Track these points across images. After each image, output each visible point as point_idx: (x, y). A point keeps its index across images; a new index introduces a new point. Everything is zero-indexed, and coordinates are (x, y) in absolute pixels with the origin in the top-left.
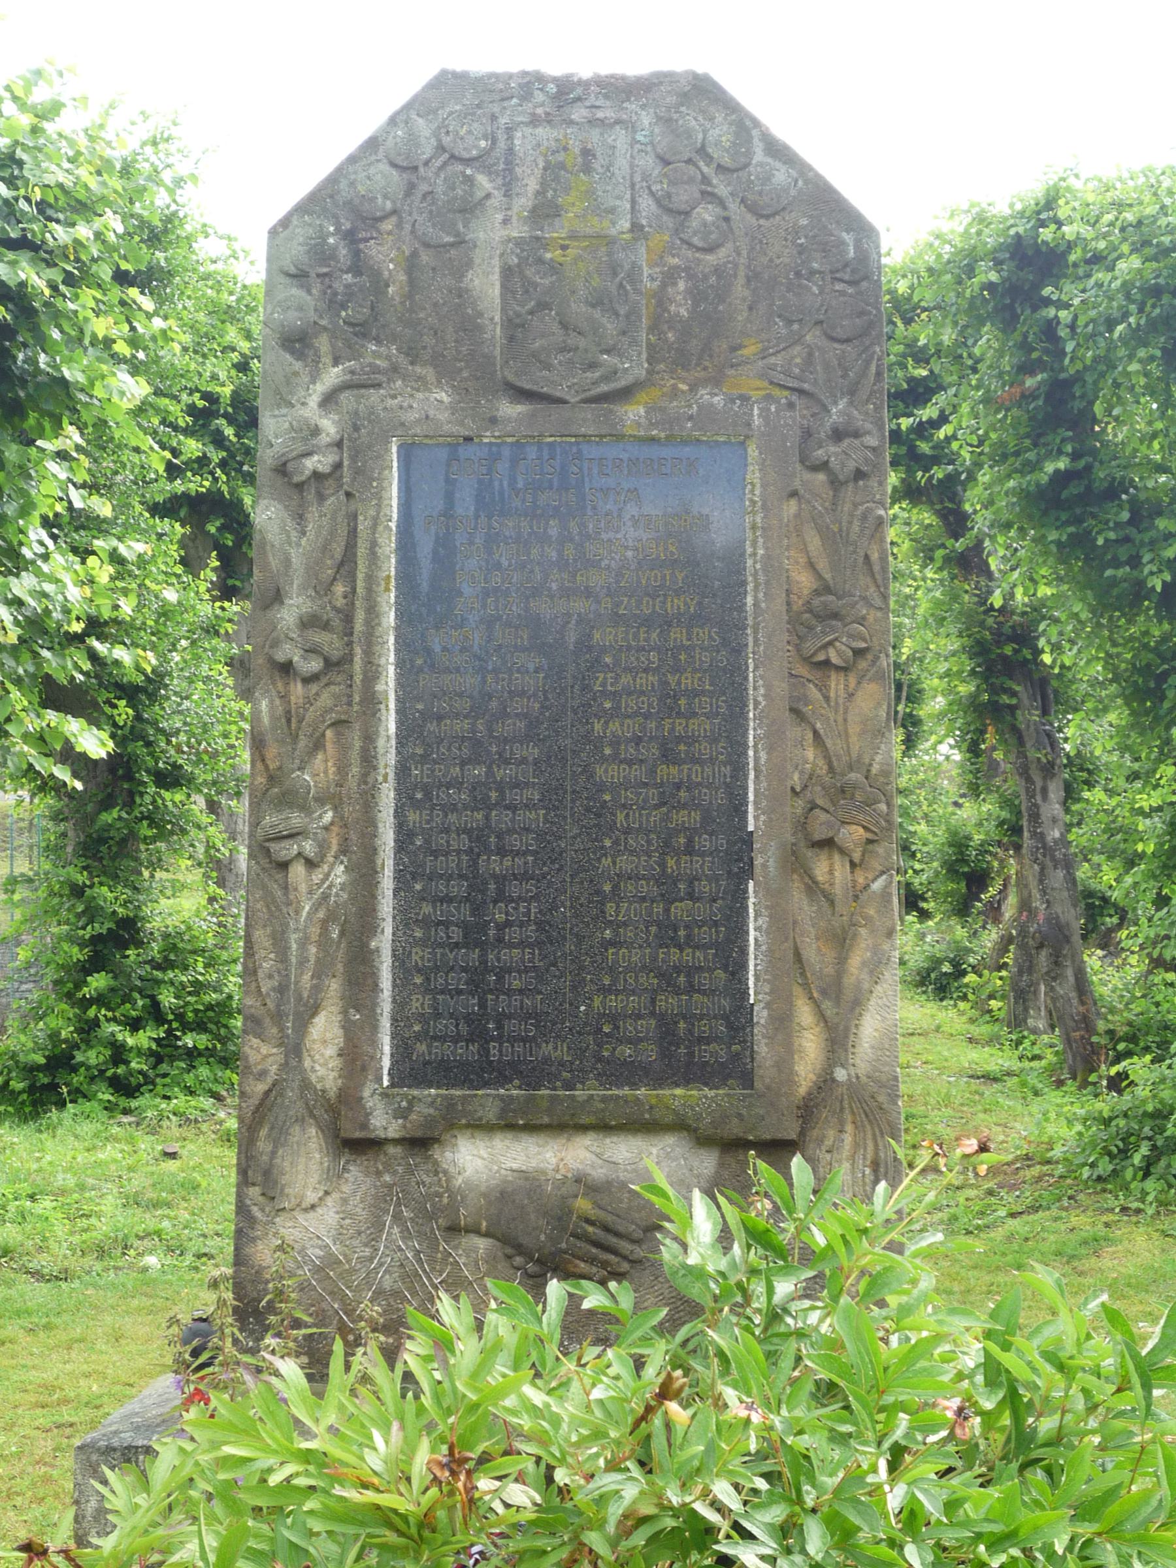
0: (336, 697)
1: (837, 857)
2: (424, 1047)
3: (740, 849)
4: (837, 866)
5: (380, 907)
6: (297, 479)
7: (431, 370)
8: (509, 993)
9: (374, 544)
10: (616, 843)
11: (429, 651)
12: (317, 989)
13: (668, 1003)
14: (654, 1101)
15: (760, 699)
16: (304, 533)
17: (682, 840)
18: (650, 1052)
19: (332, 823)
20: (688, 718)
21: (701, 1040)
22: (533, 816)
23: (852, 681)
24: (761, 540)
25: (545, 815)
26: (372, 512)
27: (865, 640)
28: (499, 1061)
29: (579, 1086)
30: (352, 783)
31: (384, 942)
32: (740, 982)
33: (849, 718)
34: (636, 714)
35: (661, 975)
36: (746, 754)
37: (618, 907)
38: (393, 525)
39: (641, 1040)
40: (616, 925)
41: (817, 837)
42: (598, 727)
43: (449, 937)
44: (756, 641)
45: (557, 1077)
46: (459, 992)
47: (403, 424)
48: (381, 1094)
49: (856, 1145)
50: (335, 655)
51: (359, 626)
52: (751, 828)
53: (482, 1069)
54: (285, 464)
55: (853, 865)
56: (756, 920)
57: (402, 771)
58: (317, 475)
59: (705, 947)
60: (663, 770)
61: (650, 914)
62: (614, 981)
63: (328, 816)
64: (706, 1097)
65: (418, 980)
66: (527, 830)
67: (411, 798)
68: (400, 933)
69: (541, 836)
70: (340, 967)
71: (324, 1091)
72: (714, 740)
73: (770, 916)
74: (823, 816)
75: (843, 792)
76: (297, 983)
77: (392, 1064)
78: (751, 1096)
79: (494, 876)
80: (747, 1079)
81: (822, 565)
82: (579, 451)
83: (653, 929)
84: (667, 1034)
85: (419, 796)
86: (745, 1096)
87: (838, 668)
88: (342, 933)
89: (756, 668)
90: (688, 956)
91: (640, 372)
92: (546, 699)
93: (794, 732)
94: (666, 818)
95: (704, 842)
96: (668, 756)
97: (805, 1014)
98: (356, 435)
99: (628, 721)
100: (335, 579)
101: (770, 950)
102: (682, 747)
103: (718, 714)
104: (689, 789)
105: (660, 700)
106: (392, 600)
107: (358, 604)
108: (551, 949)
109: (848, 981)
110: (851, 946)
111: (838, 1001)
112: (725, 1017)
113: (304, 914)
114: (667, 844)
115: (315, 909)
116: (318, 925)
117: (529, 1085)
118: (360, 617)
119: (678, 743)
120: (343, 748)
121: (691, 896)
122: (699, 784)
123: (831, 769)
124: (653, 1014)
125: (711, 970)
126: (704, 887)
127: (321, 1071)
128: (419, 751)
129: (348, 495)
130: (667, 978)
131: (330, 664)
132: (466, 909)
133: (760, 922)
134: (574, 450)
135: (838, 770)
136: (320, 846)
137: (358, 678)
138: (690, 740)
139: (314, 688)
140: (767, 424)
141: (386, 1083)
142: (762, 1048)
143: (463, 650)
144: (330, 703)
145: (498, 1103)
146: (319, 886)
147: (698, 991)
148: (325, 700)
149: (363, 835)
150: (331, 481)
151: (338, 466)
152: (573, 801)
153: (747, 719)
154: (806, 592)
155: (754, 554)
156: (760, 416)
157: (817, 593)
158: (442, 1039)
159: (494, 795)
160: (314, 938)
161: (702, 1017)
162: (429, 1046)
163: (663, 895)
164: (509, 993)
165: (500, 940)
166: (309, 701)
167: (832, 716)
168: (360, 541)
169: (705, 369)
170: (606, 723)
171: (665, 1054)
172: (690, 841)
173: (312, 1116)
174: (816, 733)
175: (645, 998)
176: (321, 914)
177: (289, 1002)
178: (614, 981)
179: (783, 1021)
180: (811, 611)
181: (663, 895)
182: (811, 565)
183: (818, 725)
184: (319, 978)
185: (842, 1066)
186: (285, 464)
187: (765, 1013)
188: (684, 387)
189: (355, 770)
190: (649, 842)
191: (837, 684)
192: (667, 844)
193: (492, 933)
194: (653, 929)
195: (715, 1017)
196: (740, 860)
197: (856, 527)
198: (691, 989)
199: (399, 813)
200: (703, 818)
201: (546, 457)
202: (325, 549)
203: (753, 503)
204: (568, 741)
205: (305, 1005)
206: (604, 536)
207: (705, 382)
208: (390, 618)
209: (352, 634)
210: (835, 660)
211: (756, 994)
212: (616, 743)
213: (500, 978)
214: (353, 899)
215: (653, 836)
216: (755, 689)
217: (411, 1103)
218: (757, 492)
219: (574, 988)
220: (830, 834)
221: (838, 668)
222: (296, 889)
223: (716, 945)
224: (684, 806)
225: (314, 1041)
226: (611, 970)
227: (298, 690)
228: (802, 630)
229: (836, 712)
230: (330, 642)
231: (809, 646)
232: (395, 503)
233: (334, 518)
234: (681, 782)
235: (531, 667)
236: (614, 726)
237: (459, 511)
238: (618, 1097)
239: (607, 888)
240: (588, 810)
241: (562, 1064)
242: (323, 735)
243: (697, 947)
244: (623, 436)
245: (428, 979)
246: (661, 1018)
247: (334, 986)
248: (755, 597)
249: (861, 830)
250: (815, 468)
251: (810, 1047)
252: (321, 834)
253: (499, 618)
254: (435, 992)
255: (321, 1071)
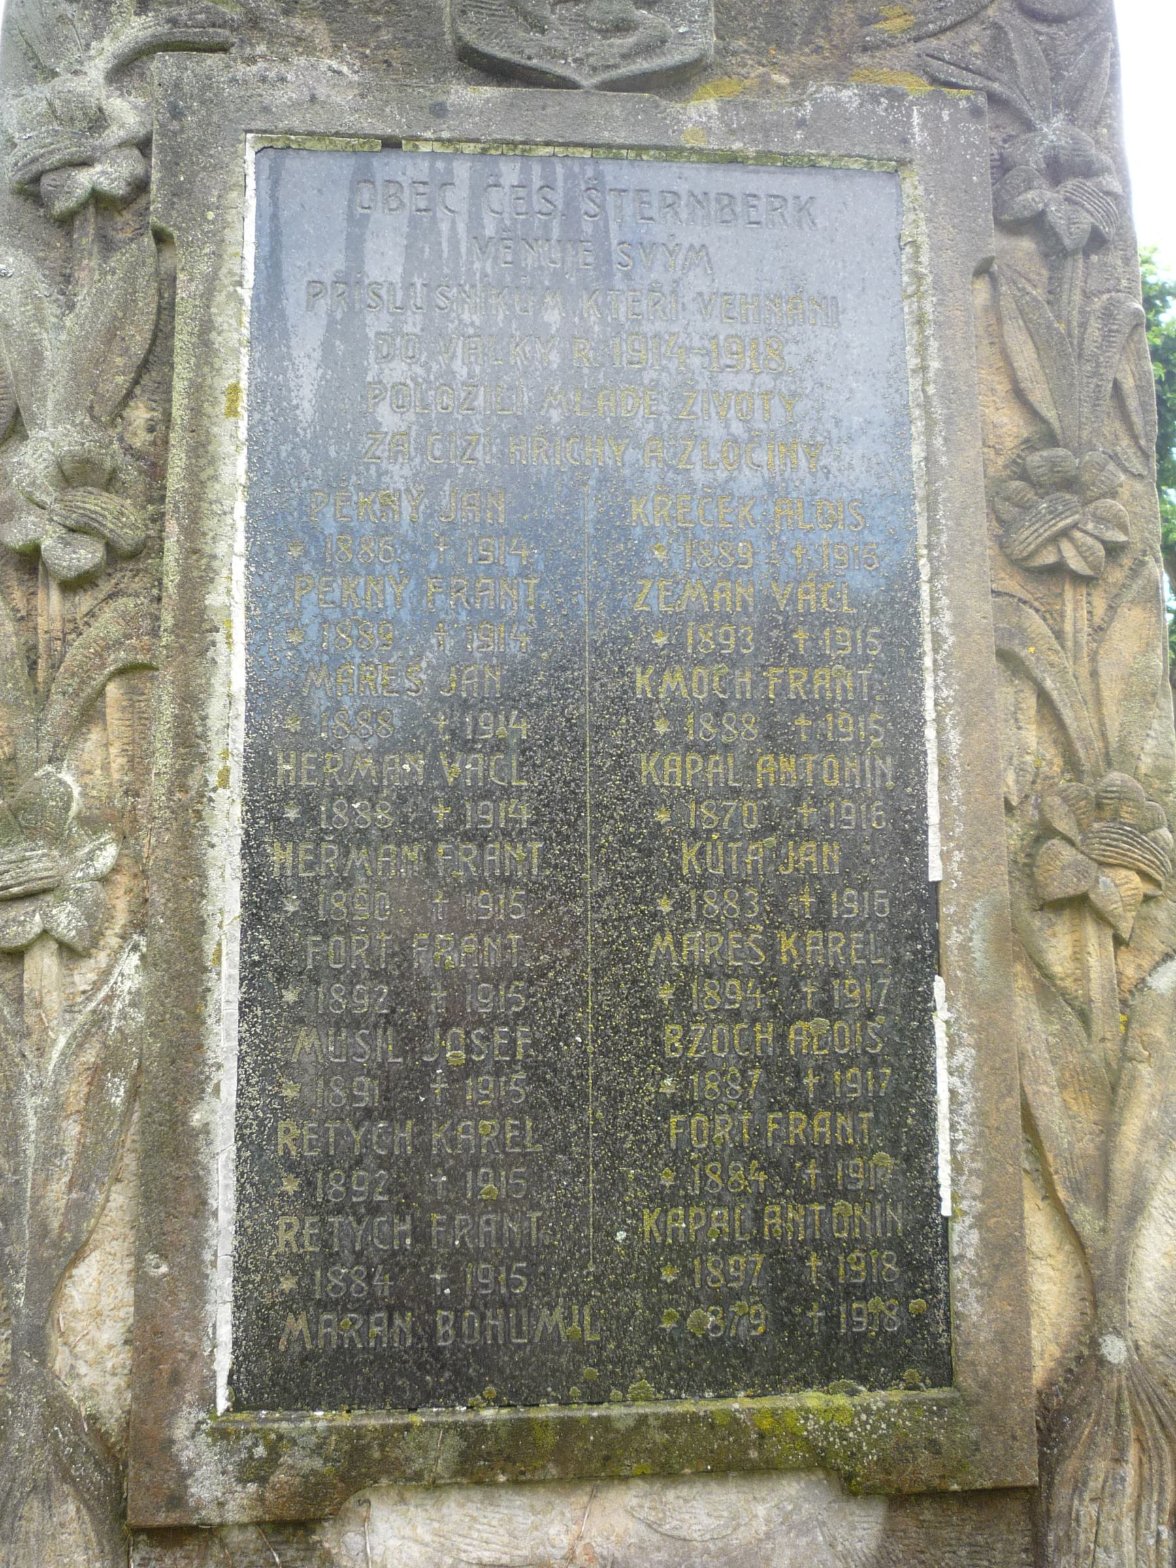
0: (128, 619)
1: (1091, 929)
2: (302, 1324)
3: (916, 916)
4: (1093, 946)
5: (211, 1041)
6: (61, 206)
7: (322, 26)
8: (474, 1208)
9: (206, 327)
10: (681, 905)
11: (313, 534)
12: (78, 1210)
13: (786, 1219)
14: (766, 1424)
15: (945, 631)
16: (71, 307)
17: (807, 900)
18: (754, 1320)
19: (116, 869)
20: (812, 667)
21: (850, 1292)
22: (519, 852)
23: (1100, 605)
24: (934, 344)
25: (543, 852)
26: (204, 267)
27: (1123, 528)
28: (455, 1349)
29: (616, 1393)
30: (157, 788)
31: (219, 1115)
32: (921, 1171)
33: (1102, 671)
34: (716, 656)
35: (771, 1165)
36: (920, 735)
37: (687, 1030)
38: (246, 293)
39: (736, 1295)
40: (684, 1069)
41: (1056, 890)
42: (641, 681)
43: (353, 1098)
44: (933, 526)
45: (572, 1377)
46: (374, 1209)
47: (266, 110)
48: (212, 1433)
49: (1143, 1485)
50: (128, 537)
51: (175, 480)
52: (935, 875)
53: (421, 1366)
54: (36, 179)
55: (1118, 941)
56: (951, 1053)
57: (259, 764)
58: (98, 199)
59: (852, 1108)
60: (766, 765)
61: (749, 1046)
62: (682, 1179)
63: (108, 856)
64: (867, 1410)
65: (290, 1186)
66: (509, 881)
67: (276, 819)
68: (253, 1091)
69: (534, 892)
70: (130, 1162)
71: (93, 1418)
72: (863, 709)
73: (978, 1047)
74: (1068, 854)
75: (1099, 806)
76: (36, 1201)
77: (237, 1362)
78: (953, 1403)
79: (444, 973)
80: (942, 1369)
81: (1039, 395)
82: (599, 176)
83: (756, 1074)
84: (785, 1284)
85: (292, 814)
86: (941, 1405)
87: (1078, 579)
88: (133, 1094)
89: (935, 574)
90: (822, 1125)
91: (706, 42)
92: (542, 626)
93: (1006, 694)
94: (776, 857)
95: (848, 904)
96: (776, 738)
97: (1040, 1231)
98: (175, 125)
99: (698, 671)
100: (129, 395)
101: (980, 1113)
102: (802, 721)
103: (866, 659)
104: (817, 801)
105: (758, 631)
106: (243, 434)
107: (174, 438)
108: (555, 1117)
109: (1122, 1166)
110: (1127, 1099)
111: (1103, 1204)
112: (896, 1244)
113: (55, 1055)
114: (778, 906)
115: (78, 1043)
116: (84, 1078)
117: (515, 1395)
118: (177, 461)
119: (795, 713)
120: (141, 721)
121: (827, 1008)
122: (836, 791)
123: (1072, 764)
124: (757, 1242)
125: (867, 1152)
126: (850, 990)
127: (89, 1376)
128: (293, 726)
129: (161, 238)
130: (783, 1170)
131: (116, 556)
132: (386, 1043)
133: (959, 1057)
134: (590, 172)
135: (1087, 767)
136: (90, 916)
137: (171, 581)
138: (820, 709)
139: (85, 602)
140: (936, 142)
141: (222, 1404)
142: (972, 1308)
143: (382, 531)
144: (115, 631)
145: (454, 1441)
146: (88, 995)
147: (844, 1195)
148: (108, 624)
149: (177, 894)
150: (127, 216)
151: (140, 186)
152: (597, 824)
153: (919, 670)
154: (1009, 443)
155: (924, 369)
156: (923, 127)
157: (1029, 445)
158: (338, 1305)
159: (441, 812)
160: (76, 1103)
161: (852, 1244)
162: (313, 1322)
163: (773, 1008)
164: (474, 1208)
165: (453, 1101)
166: (72, 627)
167: (1069, 664)
168: (179, 322)
169: (818, 50)
170: (659, 673)
171: (782, 1322)
172: (822, 900)
173: (66, 1477)
174: (1043, 697)
175: (742, 1213)
176: (90, 1055)
177: (20, 1238)
178: (682, 1179)
179: (1006, 1252)
180: (1024, 476)
181: (773, 1008)
182: (1019, 395)
183: (1049, 684)
184: (85, 1187)
185: (1117, 1333)
186: (36, 179)
187: (974, 1237)
188: (784, 80)
189: (163, 762)
190: (744, 903)
191: (1076, 609)
192: (778, 906)
193: (438, 1087)
194: (756, 1074)
195: (877, 1244)
196: (915, 937)
197: (1094, 330)
198: (831, 1191)
199: (251, 848)
200: (845, 857)
201: (537, 182)
202: (111, 334)
203: (918, 277)
204: (586, 708)
205: (55, 1245)
206: (647, 328)
207: (820, 71)
208: (235, 469)
209: (162, 499)
210: (1075, 563)
211: (955, 1199)
212: (677, 711)
213: (455, 1178)
214: (155, 1025)
215: (750, 892)
216: (934, 612)
217: (274, 1452)
218: (924, 259)
219: (603, 1196)
220: (1084, 887)
221: (1078, 579)
222: (39, 1005)
223: (875, 1102)
224: (809, 834)
225: (75, 1314)
226: (678, 1158)
227: (52, 606)
228: (1008, 510)
229: (1076, 658)
230: (120, 514)
231: (1026, 537)
232: (250, 252)
233: (130, 279)
234: (802, 787)
235: (513, 565)
236: (672, 681)
237: (374, 272)
238: (695, 1418)
239: (666, 994)
240: (626, 841)
241: (580, 1348)
242: (101, 693)
243: (840, 1108)
244: (681, 150)
245: (310, 1184)
246: (774, 1250)
247: (118, 1202)
248: (929, 445)
249: (1136, 879)
250: (1013, 227)
251: (1051, 1287)
252: (92, 891)
253: (450, 472)
254: (322, 1210)
255: (89, 1376)
